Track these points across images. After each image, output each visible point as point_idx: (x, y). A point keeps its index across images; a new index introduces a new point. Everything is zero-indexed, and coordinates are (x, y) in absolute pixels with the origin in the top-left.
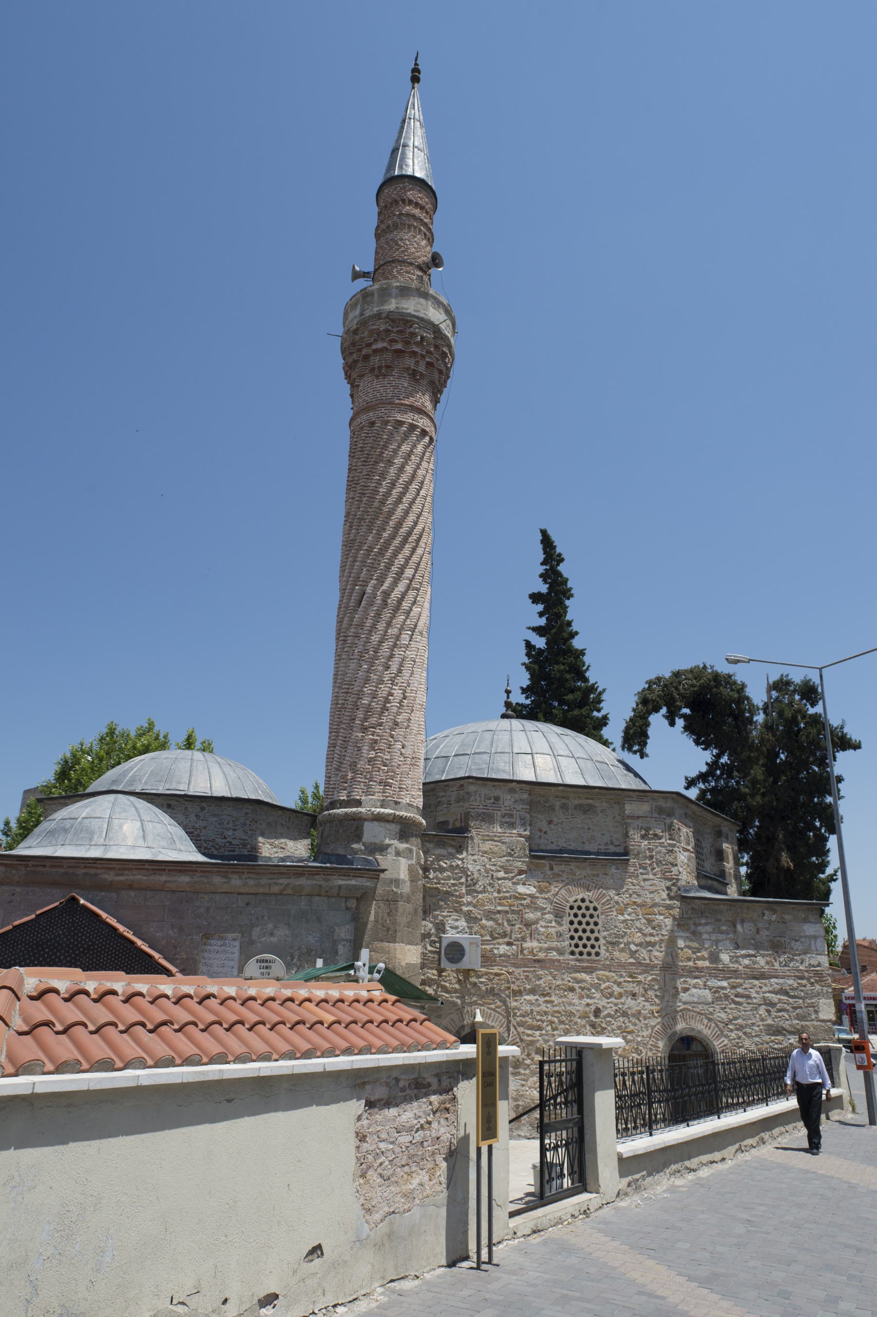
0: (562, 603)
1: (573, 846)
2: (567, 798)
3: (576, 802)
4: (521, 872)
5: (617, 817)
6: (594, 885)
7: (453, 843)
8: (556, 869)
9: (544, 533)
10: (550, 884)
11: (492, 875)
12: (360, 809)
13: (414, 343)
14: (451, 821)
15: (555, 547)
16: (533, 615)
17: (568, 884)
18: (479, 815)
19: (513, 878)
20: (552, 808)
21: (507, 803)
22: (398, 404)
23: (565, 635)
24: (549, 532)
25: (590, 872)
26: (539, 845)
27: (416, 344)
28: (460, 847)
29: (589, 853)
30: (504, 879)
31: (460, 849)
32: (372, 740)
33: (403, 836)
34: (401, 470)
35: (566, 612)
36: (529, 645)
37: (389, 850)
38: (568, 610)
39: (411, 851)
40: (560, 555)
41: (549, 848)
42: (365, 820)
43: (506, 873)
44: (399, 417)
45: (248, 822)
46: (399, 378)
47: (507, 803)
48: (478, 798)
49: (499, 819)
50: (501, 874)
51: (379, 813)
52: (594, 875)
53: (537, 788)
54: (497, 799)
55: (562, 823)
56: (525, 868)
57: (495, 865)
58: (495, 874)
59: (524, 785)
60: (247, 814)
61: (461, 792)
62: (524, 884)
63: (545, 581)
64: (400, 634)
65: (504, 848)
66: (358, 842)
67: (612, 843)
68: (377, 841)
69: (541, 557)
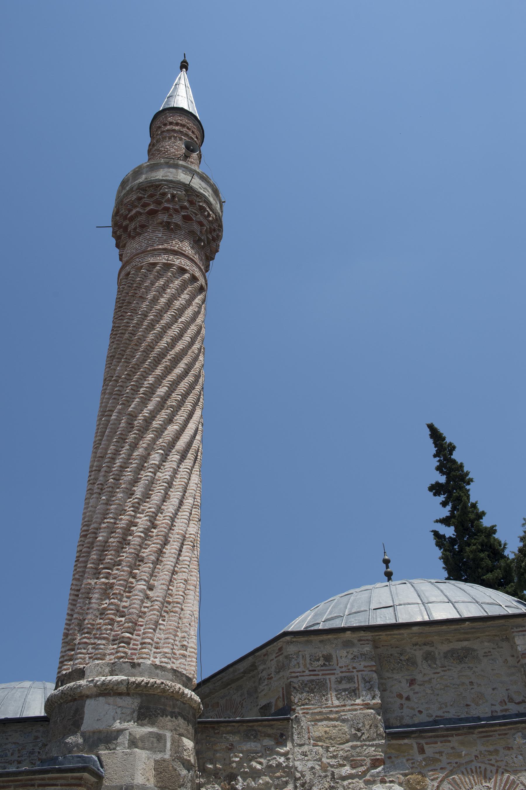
0: (461, 488)
1: (452, 713)
2: (431, 644)
3: (445, 648)
4: (375, 763)
5: (510, 659)
6: (494, 769)
7: (270, 731)
8: (429, 750)
9: (431, 427)
10: (424, 776)
11: (333, 774)
12: (83, 682)
13: (165, 202)
14: (273, 701)
15: (444, 439)
16: (437, 508)
17: (452, 773)
18: (304, 685)
19: (365, 773)
20: (412, 662)
21: (343, 662)
22: (151, 250)
23: (472, 516)
24: (436, 425)
25: (483, 748)
26: (402, 718)
27: (168, 201)
28: (282, 735)
29: (479, 719)
30: (351, 776)
31: (282, 739)
32: (106, 584)
33: (144, 715)
34: (155, 300)
35: (468, 497)
36: (436, 534)
37: (120, 739)
38: (470, 493)
39: (160, 738)
40: (450, 444)
41: (416, 720)
42: (88, 697)
43: (353, 767)
44: (152, 260)
45: (37, 749)
46: (153, 232)
47: (343, 662)
48: (301, 662)
49: (334, 686)
50: (347, 770)
51: (103, 683)
52: (490, 753)
53: (383, 635)
54: (328, 658)
55: (430, 681)
56: (380, 755)
57: (335, 757)
58: (336, 771)
59: (362, 634)
60: (37, 738)
61: (281, 658)
62: (383, 782)
63: (442, 473)
64: (149, 454)
65: (346, 728)
66: (74, 733)
67: (511, 700)
68: (101, 726)
69: (434, 450)
